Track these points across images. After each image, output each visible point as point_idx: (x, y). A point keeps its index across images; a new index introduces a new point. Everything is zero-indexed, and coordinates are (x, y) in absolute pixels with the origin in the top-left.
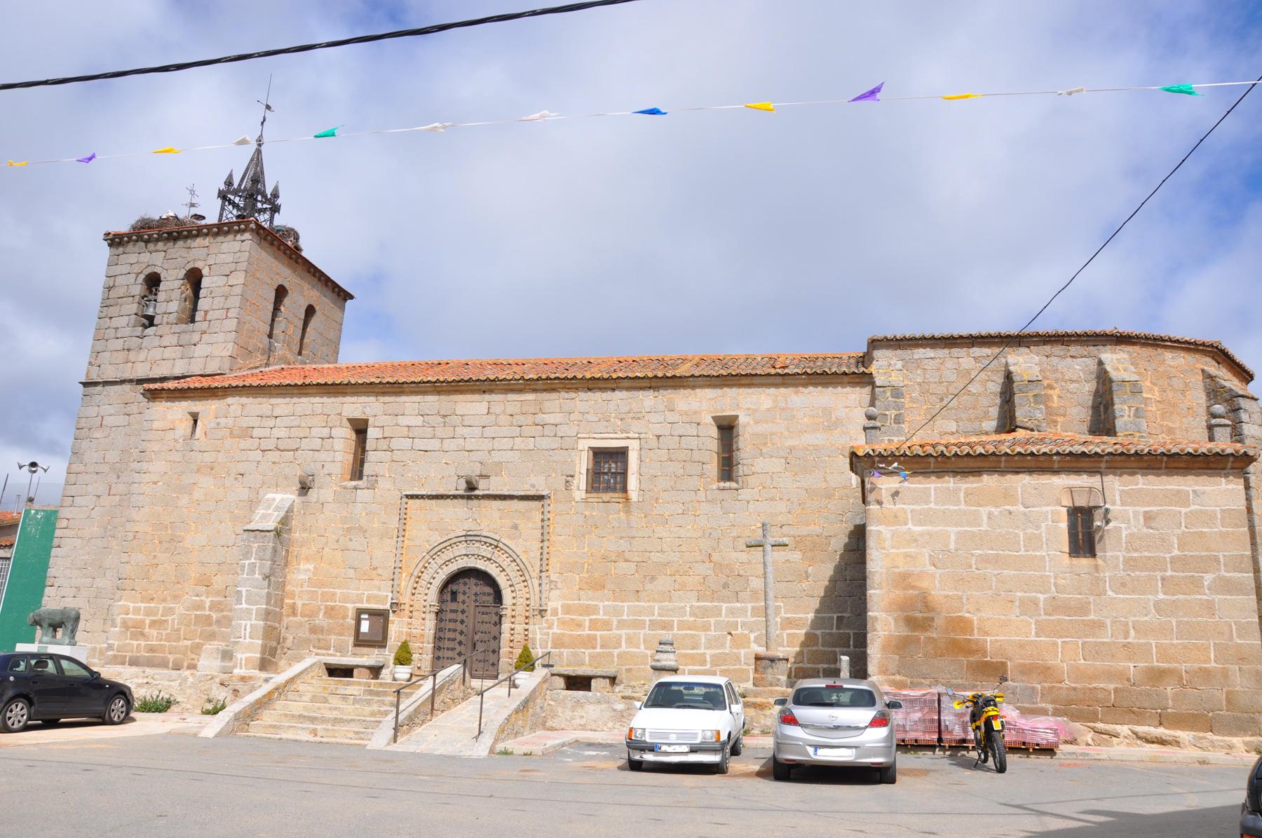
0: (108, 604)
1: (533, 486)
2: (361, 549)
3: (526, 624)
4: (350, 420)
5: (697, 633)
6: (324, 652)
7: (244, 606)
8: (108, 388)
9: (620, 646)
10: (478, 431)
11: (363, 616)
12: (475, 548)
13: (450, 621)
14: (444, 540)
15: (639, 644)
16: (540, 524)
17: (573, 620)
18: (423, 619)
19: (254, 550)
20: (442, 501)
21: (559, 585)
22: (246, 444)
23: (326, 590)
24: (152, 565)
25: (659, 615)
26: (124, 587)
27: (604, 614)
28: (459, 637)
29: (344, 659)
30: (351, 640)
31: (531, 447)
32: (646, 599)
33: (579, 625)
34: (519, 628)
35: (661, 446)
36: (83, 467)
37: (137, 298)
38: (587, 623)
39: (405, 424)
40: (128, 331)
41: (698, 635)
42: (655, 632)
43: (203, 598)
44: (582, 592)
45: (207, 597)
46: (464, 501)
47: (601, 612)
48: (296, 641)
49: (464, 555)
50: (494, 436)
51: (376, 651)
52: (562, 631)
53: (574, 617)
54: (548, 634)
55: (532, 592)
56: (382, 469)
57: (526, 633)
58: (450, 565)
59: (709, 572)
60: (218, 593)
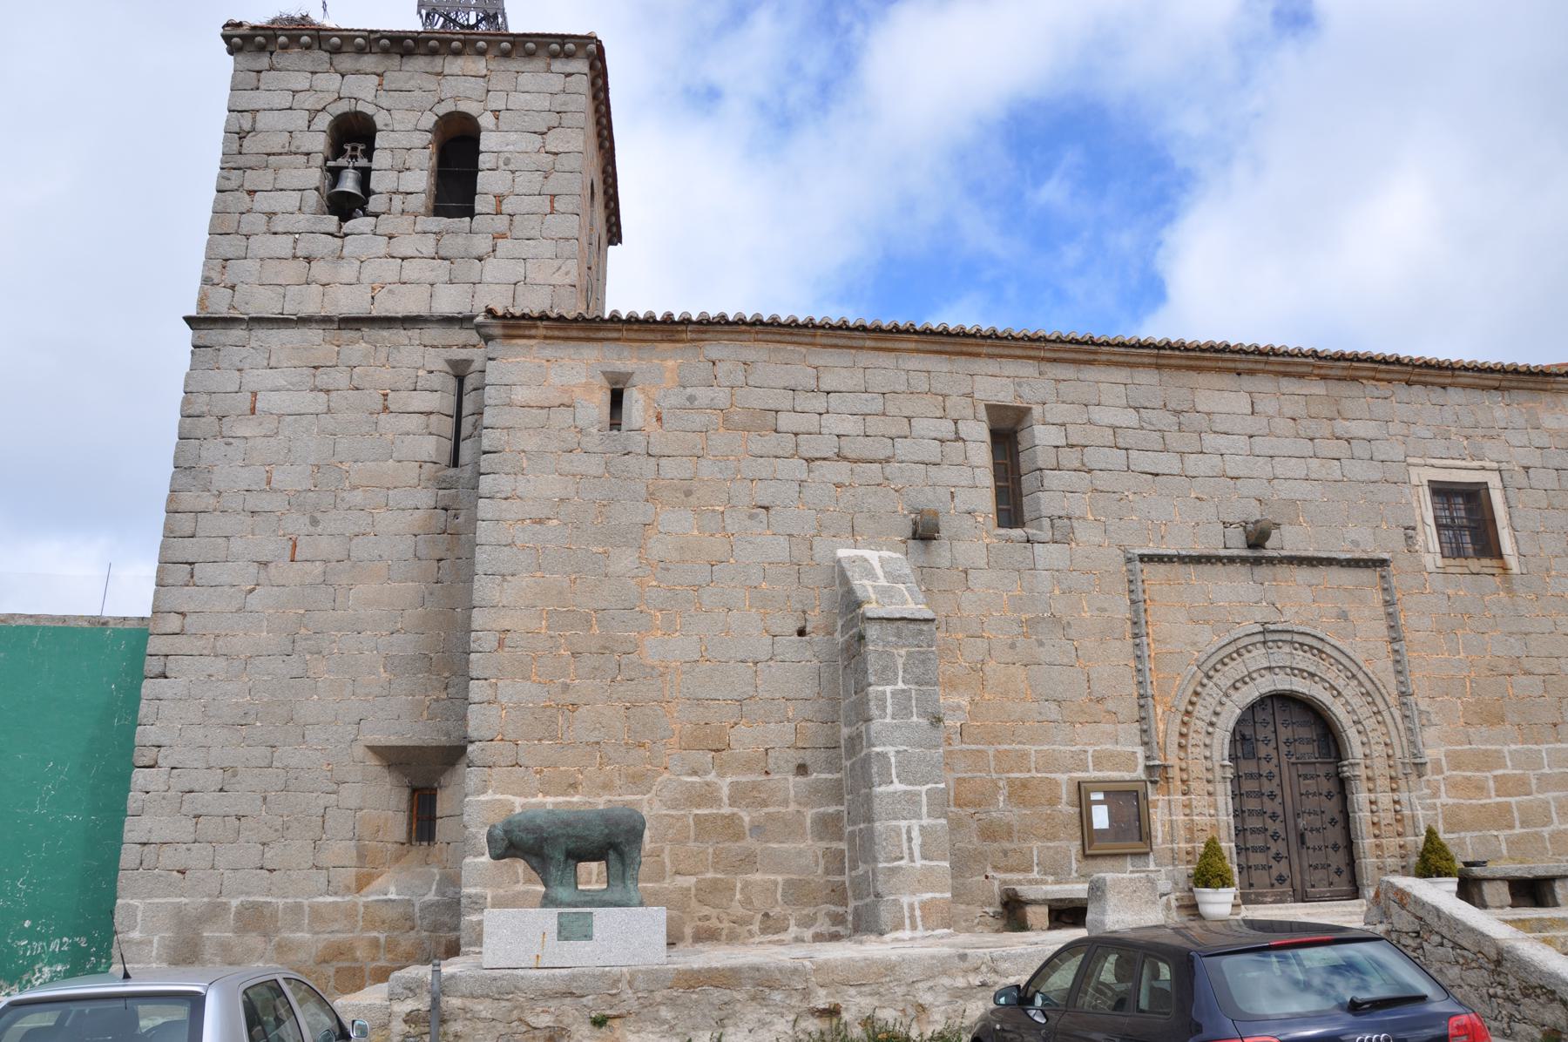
0: (322, 803)
1: (1355, 543)
2: (1066, 660)
7: (898, 786)
8: (261, 333)
9: (1551, 822)
12: (1282, 656)
16: (1381, 611)
17: (1468, 778)
19: (900, 662)
20: (1207, 568)
22: (770, 442)
23: (1006, 747)
24: (560, 707)
26: (490, 761)
27: (1514, 767)
29: (1067, 887)
30: (1075, 847)
33: (1480, 788)
34: (1385, 799)
35: (1534, 483)
36: (212, 501)
37: (319, 159)
38: (1491, 783)
39: (1106, 421)
40: (302, 221)
43: (711, 777)
44: (1471, 730)
45: (721, 775)
46: (1244, 570)
49: (1265, 669)
50: (1271, 453)
52: (1456, 801)
54: (1434, 807)
55: (1394, 733)
56: (1077, 505)
58: (1245, 689)
60: (748, 765)
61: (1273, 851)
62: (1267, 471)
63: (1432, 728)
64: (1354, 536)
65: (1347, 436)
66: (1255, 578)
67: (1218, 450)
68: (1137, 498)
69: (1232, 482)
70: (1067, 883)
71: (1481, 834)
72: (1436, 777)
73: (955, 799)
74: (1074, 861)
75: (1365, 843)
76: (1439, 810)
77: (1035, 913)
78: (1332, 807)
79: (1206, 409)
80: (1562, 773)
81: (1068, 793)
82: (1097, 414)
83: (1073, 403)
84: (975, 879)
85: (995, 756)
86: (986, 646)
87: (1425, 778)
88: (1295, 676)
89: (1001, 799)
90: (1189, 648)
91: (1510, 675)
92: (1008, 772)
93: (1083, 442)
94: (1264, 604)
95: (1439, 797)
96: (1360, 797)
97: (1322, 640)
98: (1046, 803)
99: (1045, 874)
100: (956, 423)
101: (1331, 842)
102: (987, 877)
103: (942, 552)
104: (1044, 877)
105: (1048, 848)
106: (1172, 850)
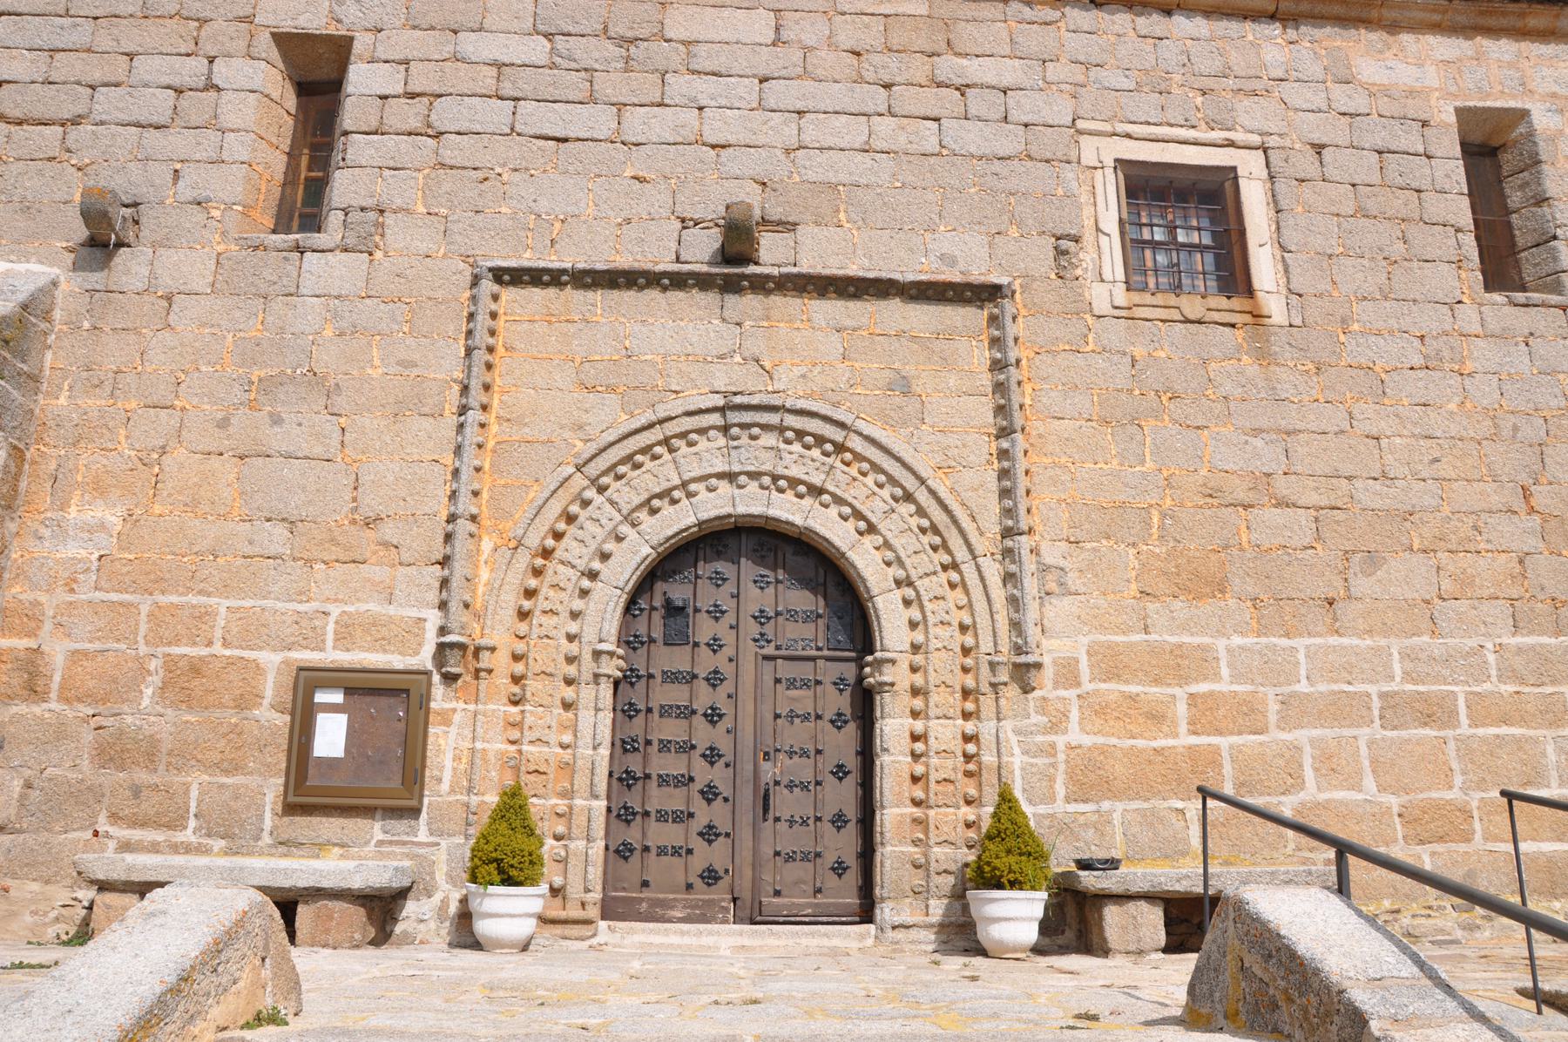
2: (318, 450)
3: (966, 716)
4: (282, 40)
5: (1532, 733)
6: (159, 836)
9: (1300, 785)
10: (746, 90)
11: (321, 697)
12: (759, 452)
13: (665, 711)
14: (637, 424)
15: (1359, 773)
16: (986, 380)
17: (1133, 698)
18: (567, 706)
20: (628, 296)
21: (1073, 580)
23: (174, 599)
25: (1408, 676)
28: (704, 773)
30: (272, 789)
31: (931, 145)
32: (1361, 625)
33: (1157, 717)
34: (945, 733)
35: (1330, 172)
38: (1182, 709)
41: (1536, 741)
42: (1404, 733)
44: (1152, 607)
46: (711, 298)
47: (1225, 672)
48: (35, 795)
49: (720, 476)
50: (800, 106)
51: (376, 829)
52: (1100, 740)
53: (1134, 689)
55: (980, 605)
56: (389, 189)
57: (971, 748)
58: (667, 510)
59: (1533, 543)
61: (700, 822)
62: (789, 134)
63: (1068, 600)
64: (946, 248)
65: (958, 81)
66: (726, 314)
67: (694, 100)
68: (517, 177)
69: (712, 153)
70: (250, 854)
71: (1146, 805)
72: (1062, 693)
73: (62, 688)
74: (268, 815)
75: (892, 814)
76: (1061, 757)
77: (108, 907)
78: (842, 745)
79: (684, 35)
80: (1334, 693)
81: (278, 686)
82: (470, 44)
83: (432, 28)
84: (72, 835)
85: (150, 615)
86: (175, 422)
87: (1037, 693)
88: (781, 491)
89: (149, 691)
90: (567, 434)
91: (1245, 507)
92: (169, 644)
93: (437, 89)
94: (738, 358)
95: (1065, 732)
96: (893, 727)
97: (842, 425)
98: (232, 704)
99: (209, 835)
100: (211, 62)
101: (828, 813)
102: (96, 834)
103: (131, 267)
104: (204, 841)
105: (222, 786)
106: (467, 805)
